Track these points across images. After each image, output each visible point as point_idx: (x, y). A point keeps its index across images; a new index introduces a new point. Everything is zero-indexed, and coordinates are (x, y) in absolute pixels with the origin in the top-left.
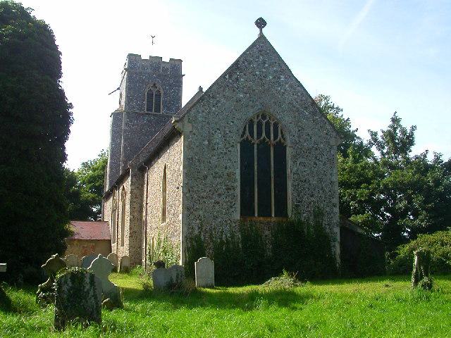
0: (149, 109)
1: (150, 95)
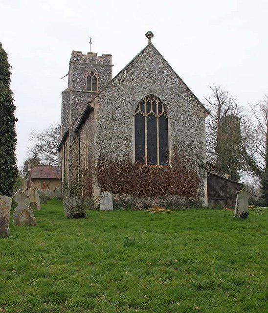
0: (89, 89)
1: (89, 79)
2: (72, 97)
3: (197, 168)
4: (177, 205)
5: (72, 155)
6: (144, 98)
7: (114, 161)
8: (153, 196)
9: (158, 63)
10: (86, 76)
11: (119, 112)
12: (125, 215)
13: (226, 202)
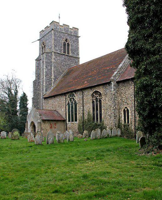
5: (116, 101)
10: (63, 42)
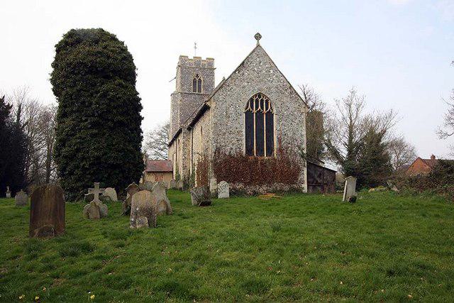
0: (195, 90)
1: (195, 81)
2: (180, 98)
3: (298, 158)
4: (281, 191)
6: (253, 97)
7: (227, 153)
8: (261, 184)
9: (265, 64)
10: (192, 79)
11: (232, 109)
12: (245, 202)
13: (323, 189)
